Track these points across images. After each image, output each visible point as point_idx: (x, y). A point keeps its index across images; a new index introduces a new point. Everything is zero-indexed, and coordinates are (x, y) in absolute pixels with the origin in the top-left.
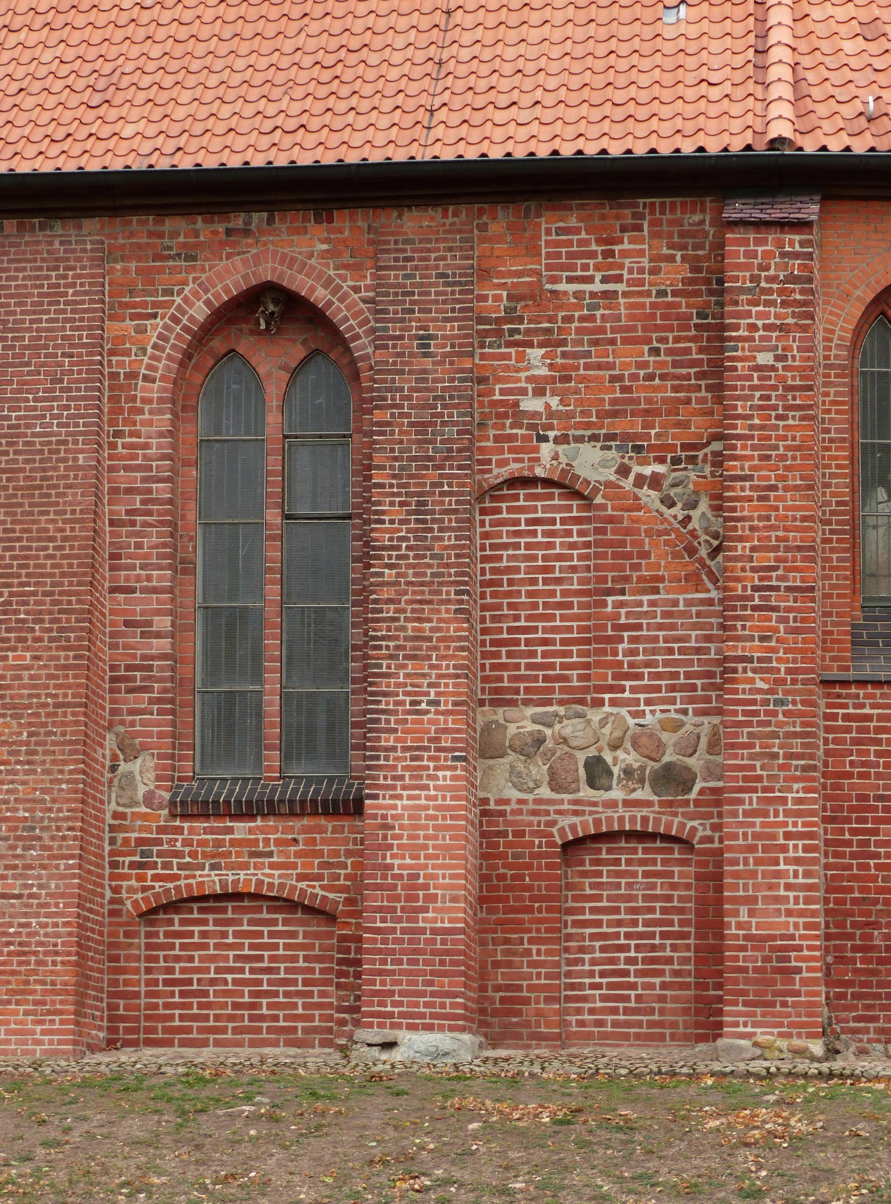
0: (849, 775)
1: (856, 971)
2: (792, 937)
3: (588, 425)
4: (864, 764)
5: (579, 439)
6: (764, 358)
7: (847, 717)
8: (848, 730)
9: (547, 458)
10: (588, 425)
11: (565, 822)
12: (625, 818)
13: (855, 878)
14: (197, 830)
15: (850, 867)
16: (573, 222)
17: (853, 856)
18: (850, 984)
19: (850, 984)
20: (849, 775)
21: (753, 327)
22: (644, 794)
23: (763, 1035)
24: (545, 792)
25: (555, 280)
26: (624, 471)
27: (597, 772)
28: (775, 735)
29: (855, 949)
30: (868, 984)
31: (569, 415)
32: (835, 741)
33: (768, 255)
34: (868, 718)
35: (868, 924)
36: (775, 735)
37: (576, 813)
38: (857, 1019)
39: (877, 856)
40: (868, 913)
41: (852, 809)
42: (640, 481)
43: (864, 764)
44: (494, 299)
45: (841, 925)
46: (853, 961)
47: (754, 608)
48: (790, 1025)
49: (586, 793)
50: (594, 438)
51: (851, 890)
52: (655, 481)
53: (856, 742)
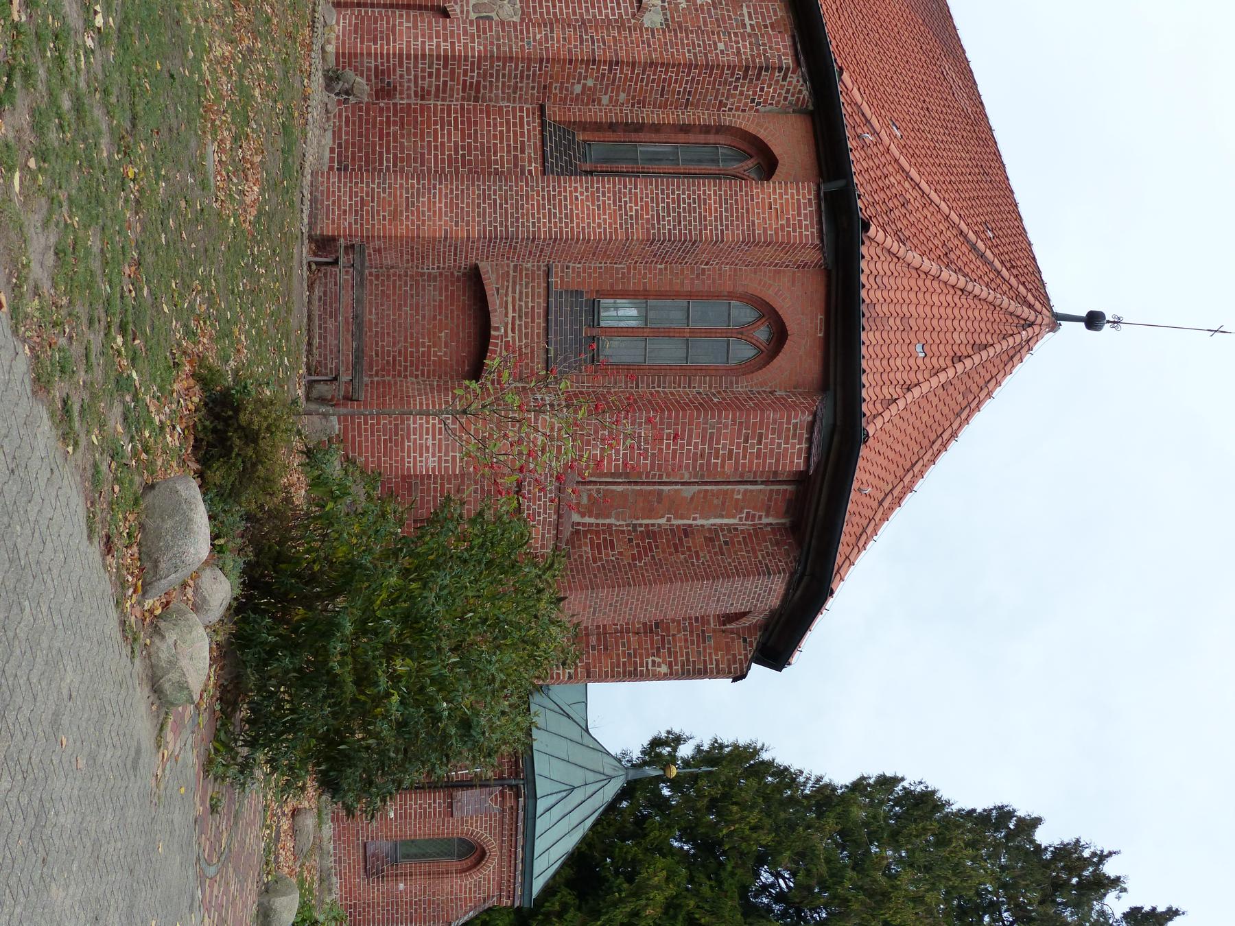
0: (488, 117)
1: (375, 117)
2: (394, 41)
3: (673, 18)
4: (495, 125)
5: (665, 14)
6: (721, 46)
7: (521, 118)
8: (515, 117)
10: (673, 18)
13: (429, 117)
15: (435, 116)
16: (780, 14)
17: (442, 118)
18: (368, 113)
19: (368, 113)
20: (488, 117)
21: (737, 42)
25: (748, 7)
28: (510, 40)
29: (388, 118)
30: (367, 122)
31: (677, 11)
32: (508, 112)
33: (779, 50)
34: (522, 127)
35: (402, 124)
36: (510, 40)
37: (462, 12)
38: (347, 117)
39: (442, 129)
40: (409, 124)
41: (469, 118)
43: (495, 125)
45: (402, 110)
46: (381, 116)
47: (581, 37)
48: (344, 42)
50: (666, 20)
51: (422, 116)
53: (508, 122)
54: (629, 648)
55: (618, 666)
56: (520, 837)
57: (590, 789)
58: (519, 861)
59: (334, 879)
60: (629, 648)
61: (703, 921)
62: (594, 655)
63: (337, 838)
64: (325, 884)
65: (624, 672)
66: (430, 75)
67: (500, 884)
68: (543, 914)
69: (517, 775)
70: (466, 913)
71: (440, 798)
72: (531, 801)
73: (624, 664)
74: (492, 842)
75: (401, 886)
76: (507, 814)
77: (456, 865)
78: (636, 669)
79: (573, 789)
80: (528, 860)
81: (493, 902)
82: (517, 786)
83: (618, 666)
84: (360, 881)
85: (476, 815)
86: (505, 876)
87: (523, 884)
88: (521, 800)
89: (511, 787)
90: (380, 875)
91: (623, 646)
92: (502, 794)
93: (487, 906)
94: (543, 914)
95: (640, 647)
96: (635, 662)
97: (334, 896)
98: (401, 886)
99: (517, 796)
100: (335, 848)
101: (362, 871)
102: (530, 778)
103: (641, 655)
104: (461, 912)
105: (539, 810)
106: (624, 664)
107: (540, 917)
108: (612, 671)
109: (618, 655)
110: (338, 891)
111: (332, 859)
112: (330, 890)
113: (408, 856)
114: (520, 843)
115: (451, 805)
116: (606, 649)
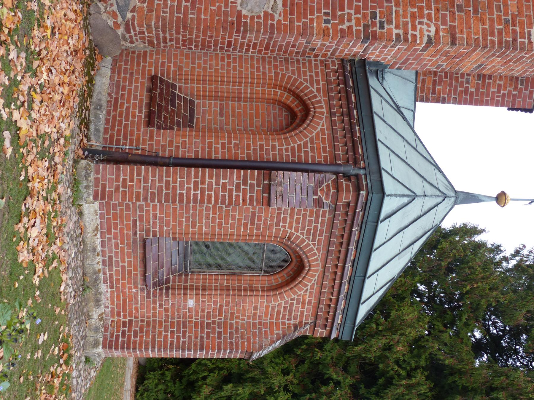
54: (506, 14)
55: (492, 34)
56: (352, 247)
57: (430, 202)
58: (345, 280)
59: (103, 287)
60: (506, 14)
61: (447, 362)
62: (460, 17)
63: (105, 229)
64: (90, 293)
65: (500, 43)
66: (240, 83)
67: (317, 308)
68: (307, 344)
69: (356, 162)
70: (273, 342)
71: (253, 177)
72: (376, 197)
73: (500, 32)
74: (315, 256)
75: (191, 303)
76: (340, 212)
77: (264, 280)
78: (515, 40)
79: (415, 196)
80: (358, 280)
81: (306, 330)
82: (357, 176)
83: (492, 34)
84: (135, 291)
85: (297, 214)
86: (325, 298)
87: (345, 312)
88: (363, 193)
89: (347, 177)
90: (164, 286)
91: (499, 9)
92: (337, 185)
93: (297, 334)
94: (307, 344)
95: (520, 13)
96: (514, 32)
97: (102, 309)
98: (191, 303)
99: (358, 189)
100: (103, 244)
101: (140, 278)
102: (374, 168)
103: (522, 24)
104: (265, 342)
105: (386, 210)
106: (500, 32)
107: (304, 347)
108: (484, 39)
109: (492, 20)
110: (108, 303)
111: (100, 259)
112: (98, 302)
113: (201, 265)
114: (351, 256)
115: (268, 189)
116: (476, 11)
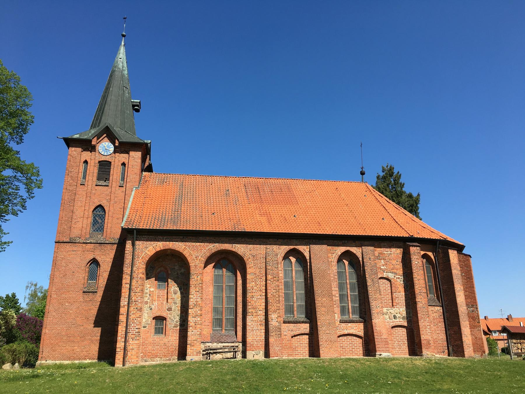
6: (416, 263)
9: (385, 275)
11: (391, 324)
12: (400, 324)
14: (343, 325)
22: (401, 320)
23: (427, 353)
24: (388, 320)
26: (395, 277)
27: (395, 317)
42: (397, 278)
44: (377, 254)
49: (394, 320)
52: (399, 278)
